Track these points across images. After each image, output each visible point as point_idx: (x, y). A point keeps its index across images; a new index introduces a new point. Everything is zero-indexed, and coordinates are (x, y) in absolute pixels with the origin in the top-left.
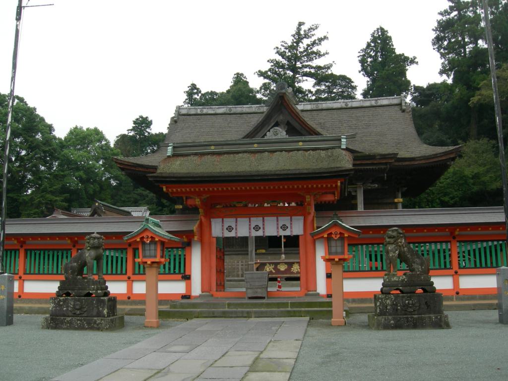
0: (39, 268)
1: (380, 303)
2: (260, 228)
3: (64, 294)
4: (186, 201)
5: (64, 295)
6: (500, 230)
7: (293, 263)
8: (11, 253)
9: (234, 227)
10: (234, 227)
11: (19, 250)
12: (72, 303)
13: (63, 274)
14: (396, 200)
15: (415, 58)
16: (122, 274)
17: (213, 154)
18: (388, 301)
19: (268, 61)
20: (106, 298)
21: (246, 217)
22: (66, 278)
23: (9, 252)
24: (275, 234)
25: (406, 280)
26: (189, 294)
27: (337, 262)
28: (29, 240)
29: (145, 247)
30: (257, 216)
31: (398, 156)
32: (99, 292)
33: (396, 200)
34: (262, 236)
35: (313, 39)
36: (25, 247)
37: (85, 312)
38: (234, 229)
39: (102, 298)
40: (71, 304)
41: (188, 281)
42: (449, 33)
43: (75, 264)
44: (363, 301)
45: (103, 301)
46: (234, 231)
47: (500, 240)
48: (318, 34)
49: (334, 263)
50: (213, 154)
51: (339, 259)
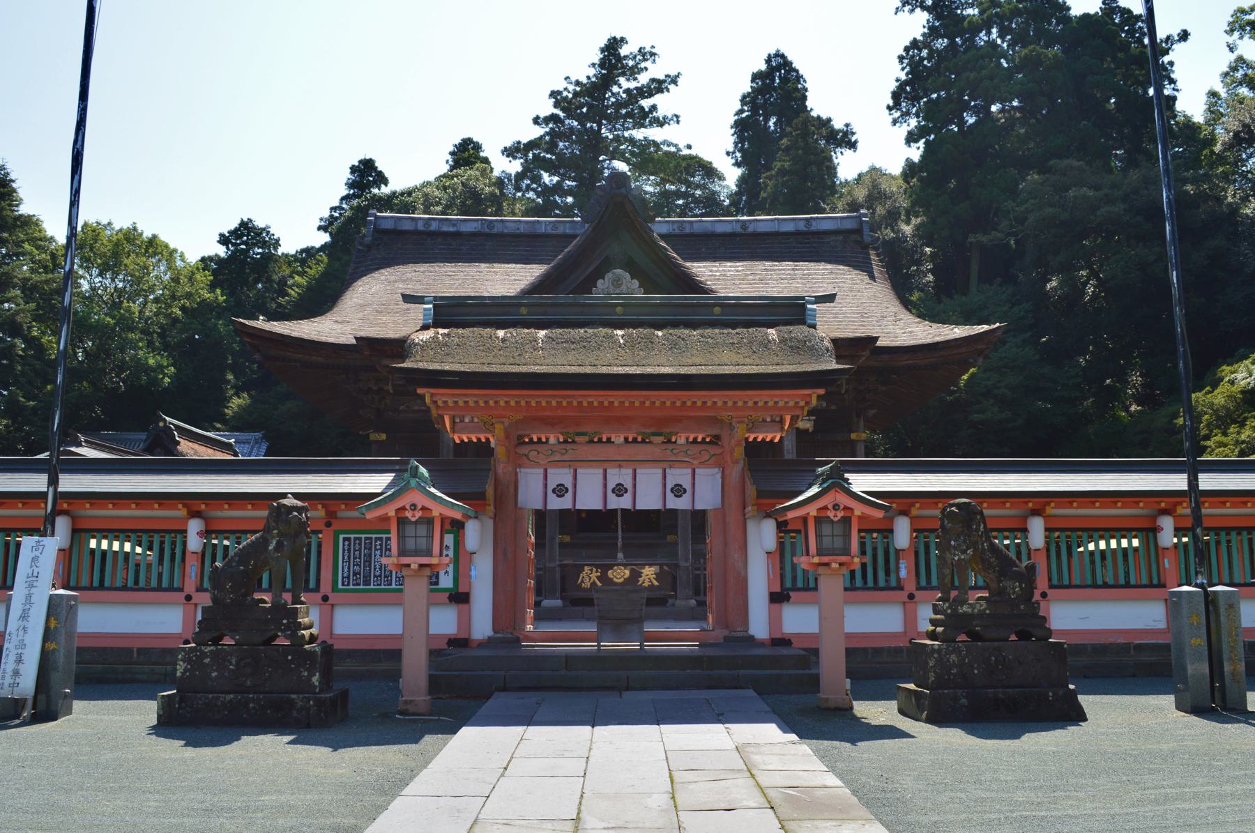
0: (102, 571)
13: (206, 590)
14: (853, 436)
15: (613, 46)
16: (171, 589)
19: (674, 81)
22: (214, 599)
24: (597, 505)
26: (466, 636)
27: (835, 570)
29: (404, 530)
31: (879, 343)
33: (853, 436)
35: (643, 79)
38: (669, 488)
41: (464, 607)
42: (925, 85)
47: (875, 531)
48: (654, 71)
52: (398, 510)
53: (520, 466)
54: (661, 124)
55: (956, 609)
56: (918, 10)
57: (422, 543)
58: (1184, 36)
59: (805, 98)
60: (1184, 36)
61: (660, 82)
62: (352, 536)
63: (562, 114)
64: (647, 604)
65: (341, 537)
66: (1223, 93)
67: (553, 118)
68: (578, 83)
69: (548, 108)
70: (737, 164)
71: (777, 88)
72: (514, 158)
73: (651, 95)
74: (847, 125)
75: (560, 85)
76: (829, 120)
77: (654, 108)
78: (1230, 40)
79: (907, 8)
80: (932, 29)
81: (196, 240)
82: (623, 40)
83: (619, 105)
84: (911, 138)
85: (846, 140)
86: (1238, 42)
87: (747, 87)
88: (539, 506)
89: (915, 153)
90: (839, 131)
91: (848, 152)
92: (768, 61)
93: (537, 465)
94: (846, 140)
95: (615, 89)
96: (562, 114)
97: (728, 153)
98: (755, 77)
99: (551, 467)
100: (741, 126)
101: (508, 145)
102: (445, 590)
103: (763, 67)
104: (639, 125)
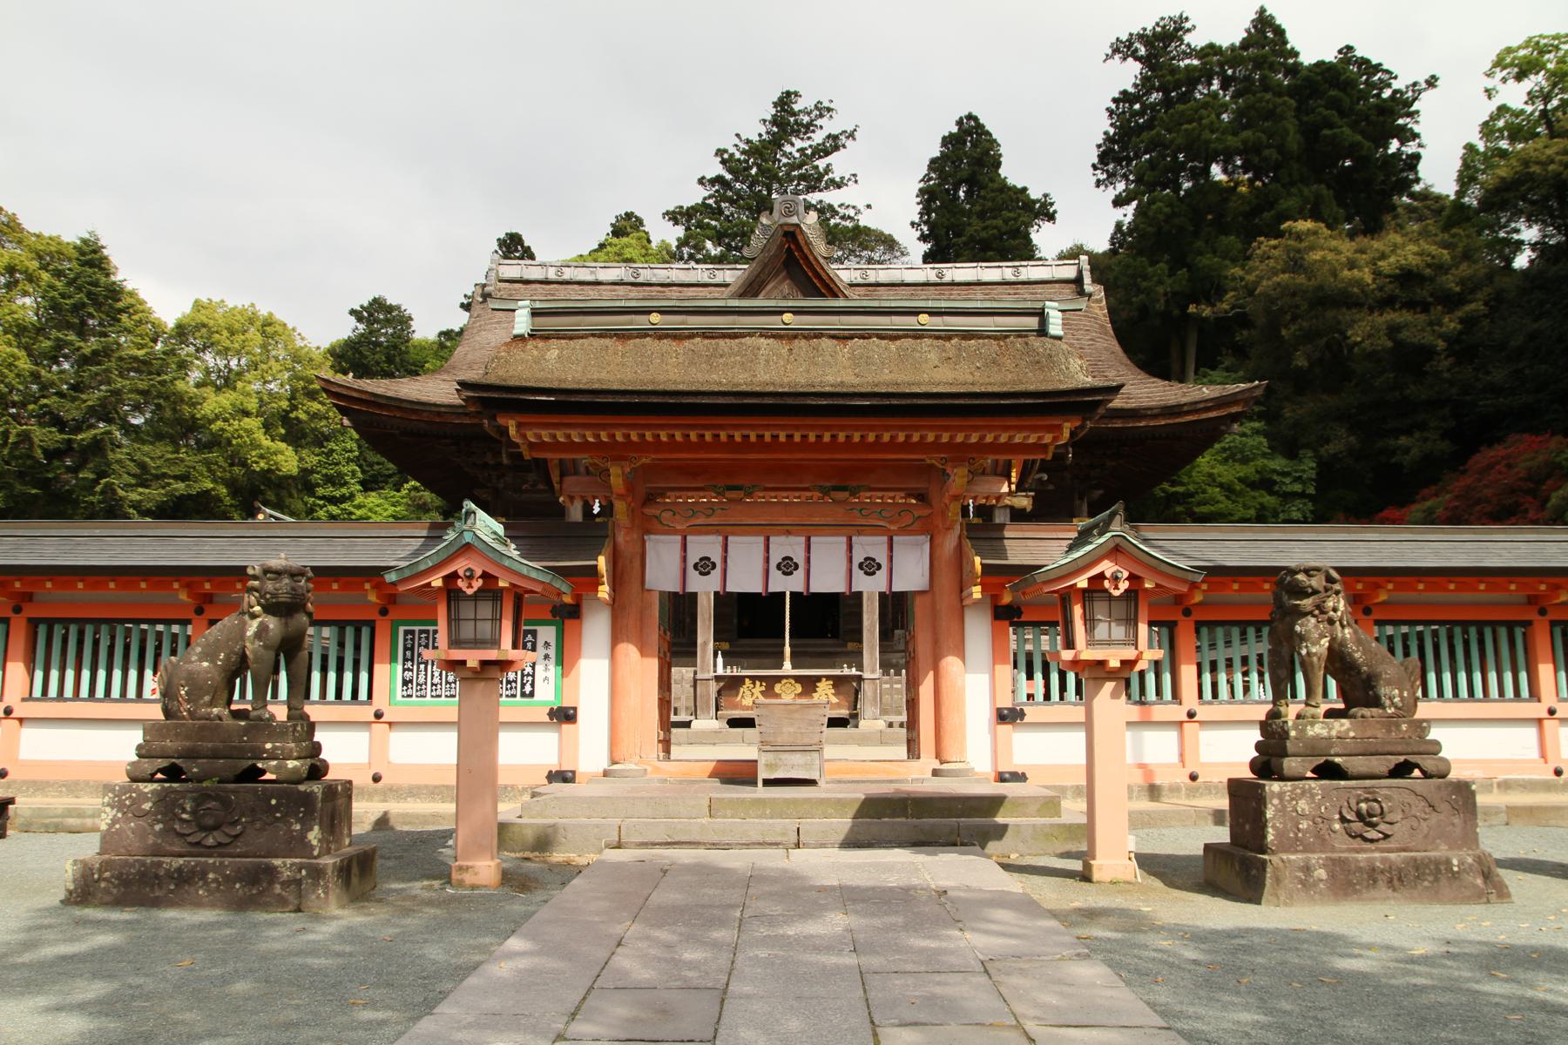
1: (1277, 810)
2: (797, 567)
3: (161, 771)
4: (561, 482)
5: (159, 776)
6: (1417, 590)
7: (819, 678)
8: (1465, 632)
9: (883, 560)
10: (883, 560)
11: (372, 625)
12: (188, 807)
15: (785, 102)
17: (660, 334)
18: (1303, 805)
19: (851, 135)
20: (316, 788)
21: (797, 534)
23: (42, 631)
24: (756, 587)
25: (1352, 734)
27: (473, 670)
28: (75, 588)
30: (875, 530)
31: (1117, 403)
32: (291, 764)
34: (759, 594)
35: (818, 137)
36: (30, 611)
37: (236, 836)
39: (302, 788)
40: (184, 811)
43: (205, 664)
44: (72, 787)
45: (308, 798)
46: (799, 574)
47: (1404, 622)
48: (828, 126)
49: (470, 675)
50: (660, 334)
51: (1123, 662)
52: (445, 578)
53: (649, 532)
54: (839, 186)
55: (1303, 731)
56: (1130, 60)
57: (485, 629)
58: (1432, 82)
59: (999, 164)
60: (1432, 82)
61: (835, 138)
62: (417, 628)
63: (728, 177)
64: (829, 726)
65: (402, 629)
66: (1481, 147)
67: (718, 180)
68: (748, 142)
69: (717, 169)
70: (923, 238)
71: (967, 160)
72: (676, 223)
73: (827, 154)
74: (1046, 196)
75: (729, 144)
76: (1025, 189)
77: (828, 169)
78: (1490, 83)
79: (1117, 57)
80: (1145, 79)
81: (324, 326)
82: (796, 94)
83: (793, 167)
84: (1118, 202)
85: (1045, 211)
86: (1500, 87)
87: (936, 151)
88: (674, 587)
89: (1128, 213)
90: (1035, 202)
91: (1046, 225)
92: (960, 123)
93: (674, 532)
94: (1045, 211)
95: (788, 148)
96: (728, 177)
97: (913, 224)
98: (946, 141)
99: (693, 533)
100: (928, 196)
101: (671, 209)
102: (543, 704)
103: (955, 129)
104: (812, 189)
